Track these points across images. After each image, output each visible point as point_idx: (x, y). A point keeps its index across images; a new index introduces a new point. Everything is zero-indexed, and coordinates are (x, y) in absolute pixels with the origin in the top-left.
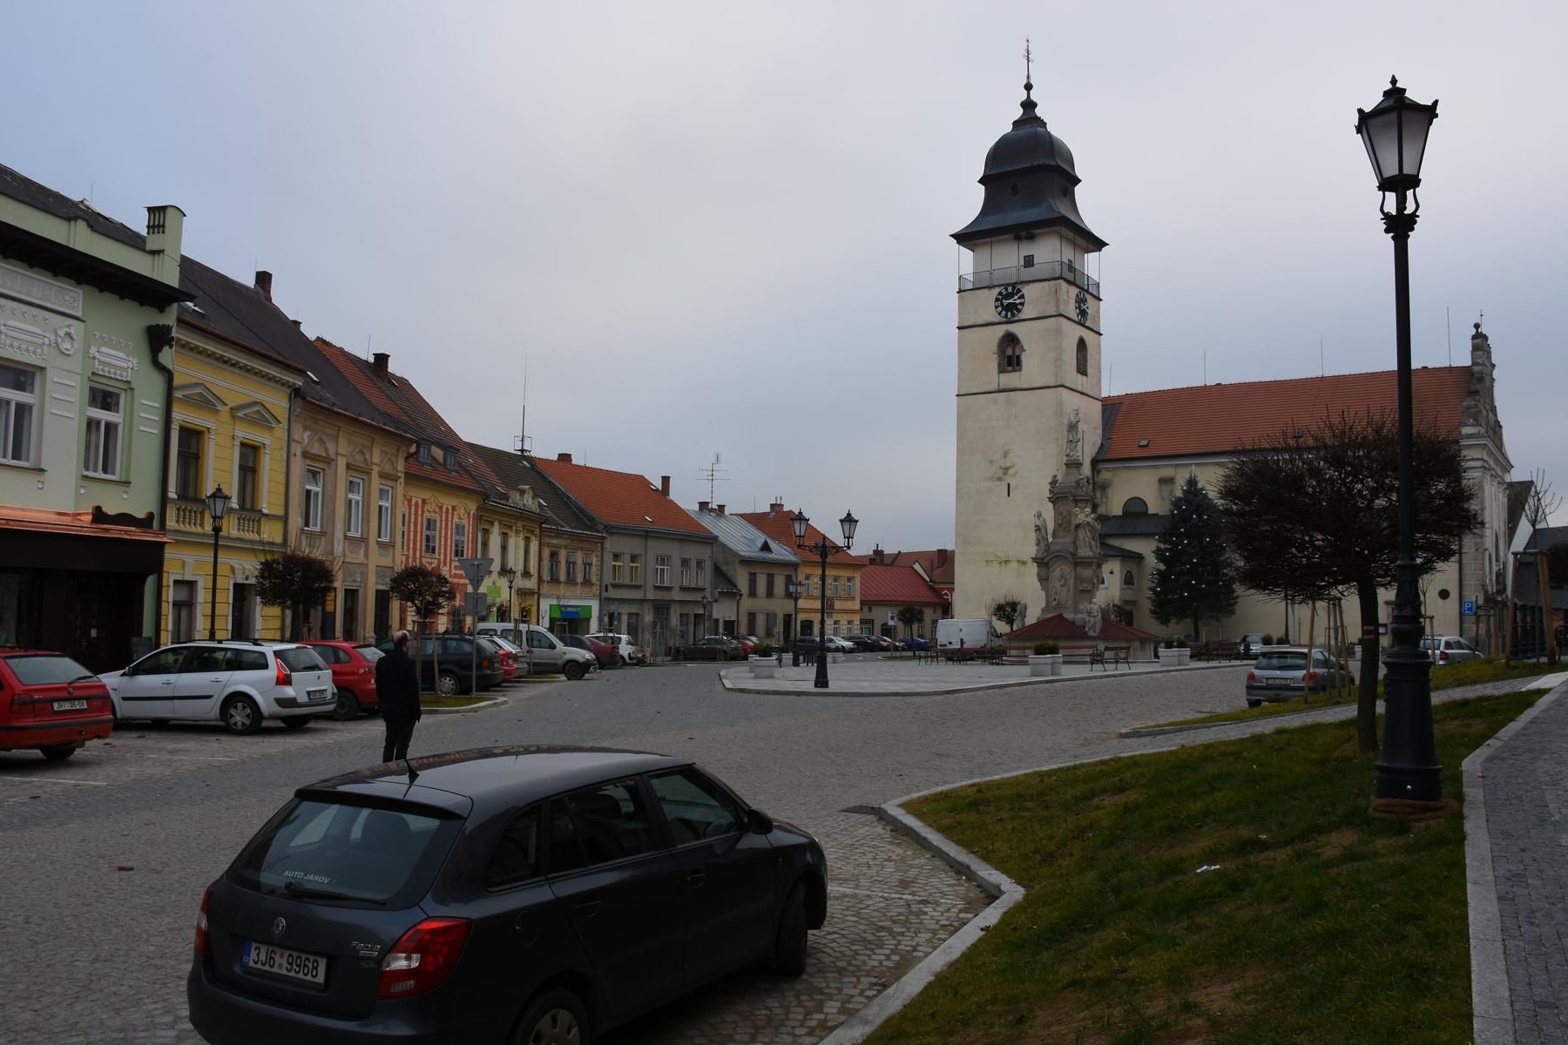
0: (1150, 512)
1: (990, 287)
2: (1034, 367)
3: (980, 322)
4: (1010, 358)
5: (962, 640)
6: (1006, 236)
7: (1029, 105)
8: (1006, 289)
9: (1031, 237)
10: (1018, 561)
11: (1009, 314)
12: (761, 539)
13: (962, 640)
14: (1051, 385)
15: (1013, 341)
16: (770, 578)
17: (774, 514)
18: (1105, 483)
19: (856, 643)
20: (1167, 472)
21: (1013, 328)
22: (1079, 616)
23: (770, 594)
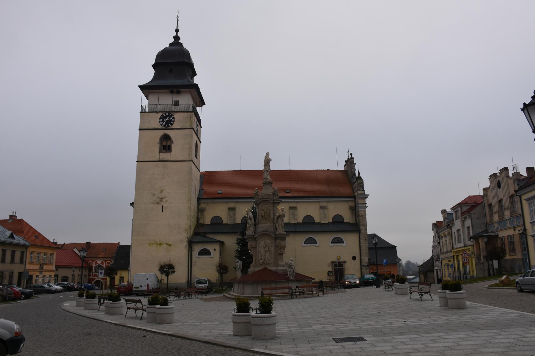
0: (223, 223)
1: (157, 112)
2: (177, 151)
3: (151, 127)
4: (164, 147)
5: (148, 284)
6: (166, 90)
7: (177, 38)
8: (166, 114)
9: (178, 93)
10: (167, 244)
11: (167, 125)
12: (9, 233)
13: (148, 284)
14: (186, 160)
15: (167, 138)
16: (13, 252)
17: (12, 220)
18: (202, 209)
19: (64, 287)
20: (232, 205)
21: (168, 132)
22: (280, 268)
23: (12, 261)
